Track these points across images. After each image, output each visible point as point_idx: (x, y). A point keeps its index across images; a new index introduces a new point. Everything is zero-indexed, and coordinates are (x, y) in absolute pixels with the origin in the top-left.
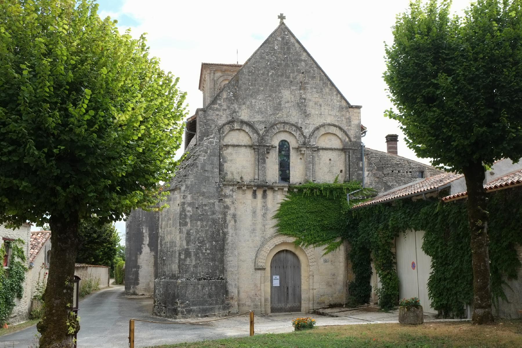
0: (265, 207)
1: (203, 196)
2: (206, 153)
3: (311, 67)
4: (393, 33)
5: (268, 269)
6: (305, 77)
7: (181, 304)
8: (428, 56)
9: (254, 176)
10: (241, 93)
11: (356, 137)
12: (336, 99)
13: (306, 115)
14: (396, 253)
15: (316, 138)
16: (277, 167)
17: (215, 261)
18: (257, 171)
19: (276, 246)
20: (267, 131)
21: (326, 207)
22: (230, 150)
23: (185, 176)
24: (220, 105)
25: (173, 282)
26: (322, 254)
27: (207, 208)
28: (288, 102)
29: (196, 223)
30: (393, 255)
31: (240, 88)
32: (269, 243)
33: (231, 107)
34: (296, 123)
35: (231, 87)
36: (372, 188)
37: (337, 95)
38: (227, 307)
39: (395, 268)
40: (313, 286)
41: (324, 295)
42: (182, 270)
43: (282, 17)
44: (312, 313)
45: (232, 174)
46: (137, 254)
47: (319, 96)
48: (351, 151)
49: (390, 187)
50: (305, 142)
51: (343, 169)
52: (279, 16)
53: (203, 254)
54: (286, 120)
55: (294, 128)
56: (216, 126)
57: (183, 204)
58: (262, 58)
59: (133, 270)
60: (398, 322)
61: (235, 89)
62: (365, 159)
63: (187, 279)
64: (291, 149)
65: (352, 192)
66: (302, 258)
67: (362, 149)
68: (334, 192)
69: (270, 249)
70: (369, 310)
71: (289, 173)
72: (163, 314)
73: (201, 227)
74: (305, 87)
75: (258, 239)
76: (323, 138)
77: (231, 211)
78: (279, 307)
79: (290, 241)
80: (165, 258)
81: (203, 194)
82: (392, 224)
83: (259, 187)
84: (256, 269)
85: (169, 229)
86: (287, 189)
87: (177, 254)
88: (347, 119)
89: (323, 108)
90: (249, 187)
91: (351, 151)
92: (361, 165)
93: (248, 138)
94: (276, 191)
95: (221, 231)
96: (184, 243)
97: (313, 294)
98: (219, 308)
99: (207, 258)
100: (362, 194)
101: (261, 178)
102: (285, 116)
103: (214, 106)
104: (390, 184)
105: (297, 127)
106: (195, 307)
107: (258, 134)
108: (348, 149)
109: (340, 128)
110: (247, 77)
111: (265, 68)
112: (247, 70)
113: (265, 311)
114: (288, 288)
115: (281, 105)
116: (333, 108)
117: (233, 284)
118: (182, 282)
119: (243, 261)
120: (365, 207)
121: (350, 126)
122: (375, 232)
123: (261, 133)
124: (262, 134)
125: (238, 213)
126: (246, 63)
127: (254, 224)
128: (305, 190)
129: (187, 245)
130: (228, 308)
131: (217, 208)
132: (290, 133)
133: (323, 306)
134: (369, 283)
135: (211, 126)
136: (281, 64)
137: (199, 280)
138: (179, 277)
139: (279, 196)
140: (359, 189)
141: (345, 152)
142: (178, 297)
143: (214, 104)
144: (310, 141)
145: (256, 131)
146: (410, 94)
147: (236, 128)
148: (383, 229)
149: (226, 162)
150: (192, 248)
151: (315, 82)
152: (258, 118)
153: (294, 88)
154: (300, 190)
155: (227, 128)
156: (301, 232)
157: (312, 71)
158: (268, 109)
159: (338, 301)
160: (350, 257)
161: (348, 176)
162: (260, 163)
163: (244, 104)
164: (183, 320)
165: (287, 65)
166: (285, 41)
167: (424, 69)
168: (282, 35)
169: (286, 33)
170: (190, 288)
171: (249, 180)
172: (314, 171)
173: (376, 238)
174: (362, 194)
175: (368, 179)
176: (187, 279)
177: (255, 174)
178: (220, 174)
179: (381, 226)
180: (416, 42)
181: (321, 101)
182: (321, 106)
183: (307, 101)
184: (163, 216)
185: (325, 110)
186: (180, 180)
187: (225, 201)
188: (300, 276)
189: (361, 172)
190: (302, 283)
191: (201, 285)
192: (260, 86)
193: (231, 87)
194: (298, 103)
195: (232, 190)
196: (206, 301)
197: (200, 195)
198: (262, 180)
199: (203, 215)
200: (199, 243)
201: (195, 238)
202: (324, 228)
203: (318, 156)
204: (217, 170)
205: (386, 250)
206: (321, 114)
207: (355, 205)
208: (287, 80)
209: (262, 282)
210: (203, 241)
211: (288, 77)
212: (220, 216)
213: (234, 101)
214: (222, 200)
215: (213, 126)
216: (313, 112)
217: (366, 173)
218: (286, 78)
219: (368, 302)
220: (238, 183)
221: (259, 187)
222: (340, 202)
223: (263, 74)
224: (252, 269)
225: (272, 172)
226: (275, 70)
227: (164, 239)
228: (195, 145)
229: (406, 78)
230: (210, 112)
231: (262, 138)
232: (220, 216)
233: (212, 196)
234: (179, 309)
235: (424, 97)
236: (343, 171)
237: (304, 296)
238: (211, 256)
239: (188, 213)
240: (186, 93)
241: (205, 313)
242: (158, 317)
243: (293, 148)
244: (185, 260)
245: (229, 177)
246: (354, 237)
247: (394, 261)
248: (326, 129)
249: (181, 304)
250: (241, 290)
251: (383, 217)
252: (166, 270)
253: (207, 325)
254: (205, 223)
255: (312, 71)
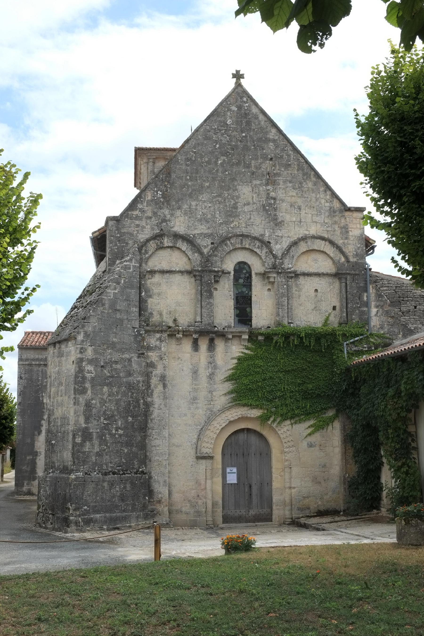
0: (212, 363)
1: (112, 348)
2: (118, 283)
3: (283, 150)
4: (368, 95)
5: (218, 457)
6: (274, 166)
7: (75, 510)
8: (417, 131)
9: (195, 317)
10: (174, 191)
11: (357, 255)
12: (324, 199)
13: (278, 223)
14: (416, 432)
15: (293, 257)
16: (231, 303)
17: (132, 445)
18: (199, 310)
19: (231, 422)
20: (215, 249)
21: (310, 362)
22: (157, 278)
23: (84, 319)
24: (143, 211)
25: (63, 478)
26: (305, 434)
27: (119, 366)
28: (248, 204)
29: (102, 389)
30: (412, 435)
31: (172, 184)
32: (219, 419)
33: (159, 214)
34: (262, 235)
35: (159, 183)
36: (383, 334)
37: (325, 191)
38: (151, 514)
39: (415, 456)
40: (290, 483)
41: (308, 497)
42: (78, 459)
43: (238, 76)
44: (289, 524)
45: (161, 314)
46: (34, 435)
47: (297, 194)
48: (348, 277)
49: (411, 332)
50: (275, 264)
51: (338, 305)
52: (233, 74)
53: (112, 436)
54: (244, 231)
55: (258, 244)
56: (135, 242)
57: (81, 360)
58: (207, 138)
59: (28, 458)
60: (395, 540)
61: (165, 186)
62: (371, 290)
63: (86, 474)
64: (254, 276)
65: (352, 341)
66: (272, 440)
67: (366, 273)
68: (323, 341)
69: (220, 428)
70: (376, 520)
71: (251, 312)
72: (50, 526)
73: (109, 395)
74: (275, 181)
75: (201, 413)
76: (304, 258)
77: (158, 371)
78: (236, 514)
79: (252, 416)
80: (53, 442)
81: (113, 346)
82: (406, 389)
83: (202, 333)
84: (198, 458)
85: (60, 399)
86: (247, 337)
87: (71, 437)
88: (341, 228)
89: (303, 212)
90: (186, 334)
91: (348, 277)
92: (365, 299)
93: (185, 259)
94: (229, 339)
95: (142, 401)
96: (82, 420)
97: (291, 495)
98: (138, 517)
99: (119, 442)
100: (368, 342)
101: (206, 320)
102: (244, 225)
103: (133, 212)
104: (411, 326)
105: (262, 242)
106: (98, 516)
107: (201, 253)
108: (344, 274)
109: (332, 243)
110: (184, 167)
111: (212, 153)
112: (184, 158)
113: (214, 521)
114: (250, 486)
115: (236, 208)
116: (320, 212)
117: (161, 480)
118: (77, 478)
119: (177, 446)
120: (368, 363)
121: (346, 238)
122: (382, 401)
123: (205, 251)
124: (208, 253)
125: (170, 373)
126: (183, 146)
127: (195, 390)
128: (275, 338)
129: (86, 422)
130: (153, 516)
131: (135, 366)
132: (252, 251)
133: (307, 513)
134: (379, 478)
135: (127, 243)
136: (236, 146)
137: (106, 474)
138: (73, 470)
139: (234, 347)
140: (362, 335)
141: (340, 279)
142: (70, 500)
143: (133, 210)
144: (282, 263)
145: (197, 248)
146: (394, 190)
147: (166, 245)
148: (393, 397)
149: (150, 296)
150: (94, 428)
151: (290, 172)
152: (202, 229)
153: (258, 182)
154: (269, 337)
155: (152, 245)
156: (271, 401)
157: (285, 156)
158: (217, 216)
159: (331, 505)
160: (348, 439)
161: (345, 315)
162: (203, 298)
163: (179, 208)
164: (77, 535)
165: (246, 148)
166: (243, 111)
167: (411, 151)
168: (239, 103)
169: (245, 99)
170: (90, 487)
171: (186, 324)
172: (289, 309)
173: (384, 410)
174: (368, 342)
175: (376, 319)
176: (86, 474)
177: (196, 314)
178: (140, 315)
179: (391, 392)
180: (398, 109)
181: (300, 201)
182: (300, 209)
183: (278, 202)
184: (53, 378)
185: (307, 214)
186: (76, 325)
187: (148, 356)
188: (270, 467)
189: (365, 309)
190: (274, 479)
191: (109, 481)
192: (204, 181)
193: (159, 183)
194: (264, 206)
195: (160, 339)
196: (117, 507)
197: (108, 348)
198: (207, 322)
199: (112, 377)
200: (105, 419)
201: (99, 411)
202: (306, 395)
203: (297, 285)
204: (135, 310)
205: (400, 429)
206: (301, 221)
207: (357, 360)
208: (247, 170)
209: (208, 477)
210: (113, 416)
211: (248, 166)
212: (140, 379)
213: (163, 204)
214: (143, 354)
215: (130, 242)
216: (288, 218)
217: (374, 310)
218: (244, 167)
219: (378, 508)
220: (170, 327)
221: (202, 333)
222: (332, 355)
223: (209, 163)
224: (191, 459)
225: (224, 310)
226: (227, 156)
227: (54, 414)
228: (104, 272)
229: (385, 164)
230: (127, 222)
231: (207, 260)
232: (140, 379)
233: (127, 349)
234: (71, 518)
235: (414, 193)
236: (338, 308)
237: (275, 498)
238: (124, 439)
239: (88, 375)
240: (40, 196)
241: (114, 524)
242: (42, 530)
243: (256, 274)
244: (82, 445)
245: (156, 318)
246: (355, 408)
247: (413, 445)
248: (309, 243)
249: (75, 510)
250: (174, 490)
251: (394, 378)
252: (55, 459)
253: (111, 542)
254: (115, 389)
255: (285, 156)
